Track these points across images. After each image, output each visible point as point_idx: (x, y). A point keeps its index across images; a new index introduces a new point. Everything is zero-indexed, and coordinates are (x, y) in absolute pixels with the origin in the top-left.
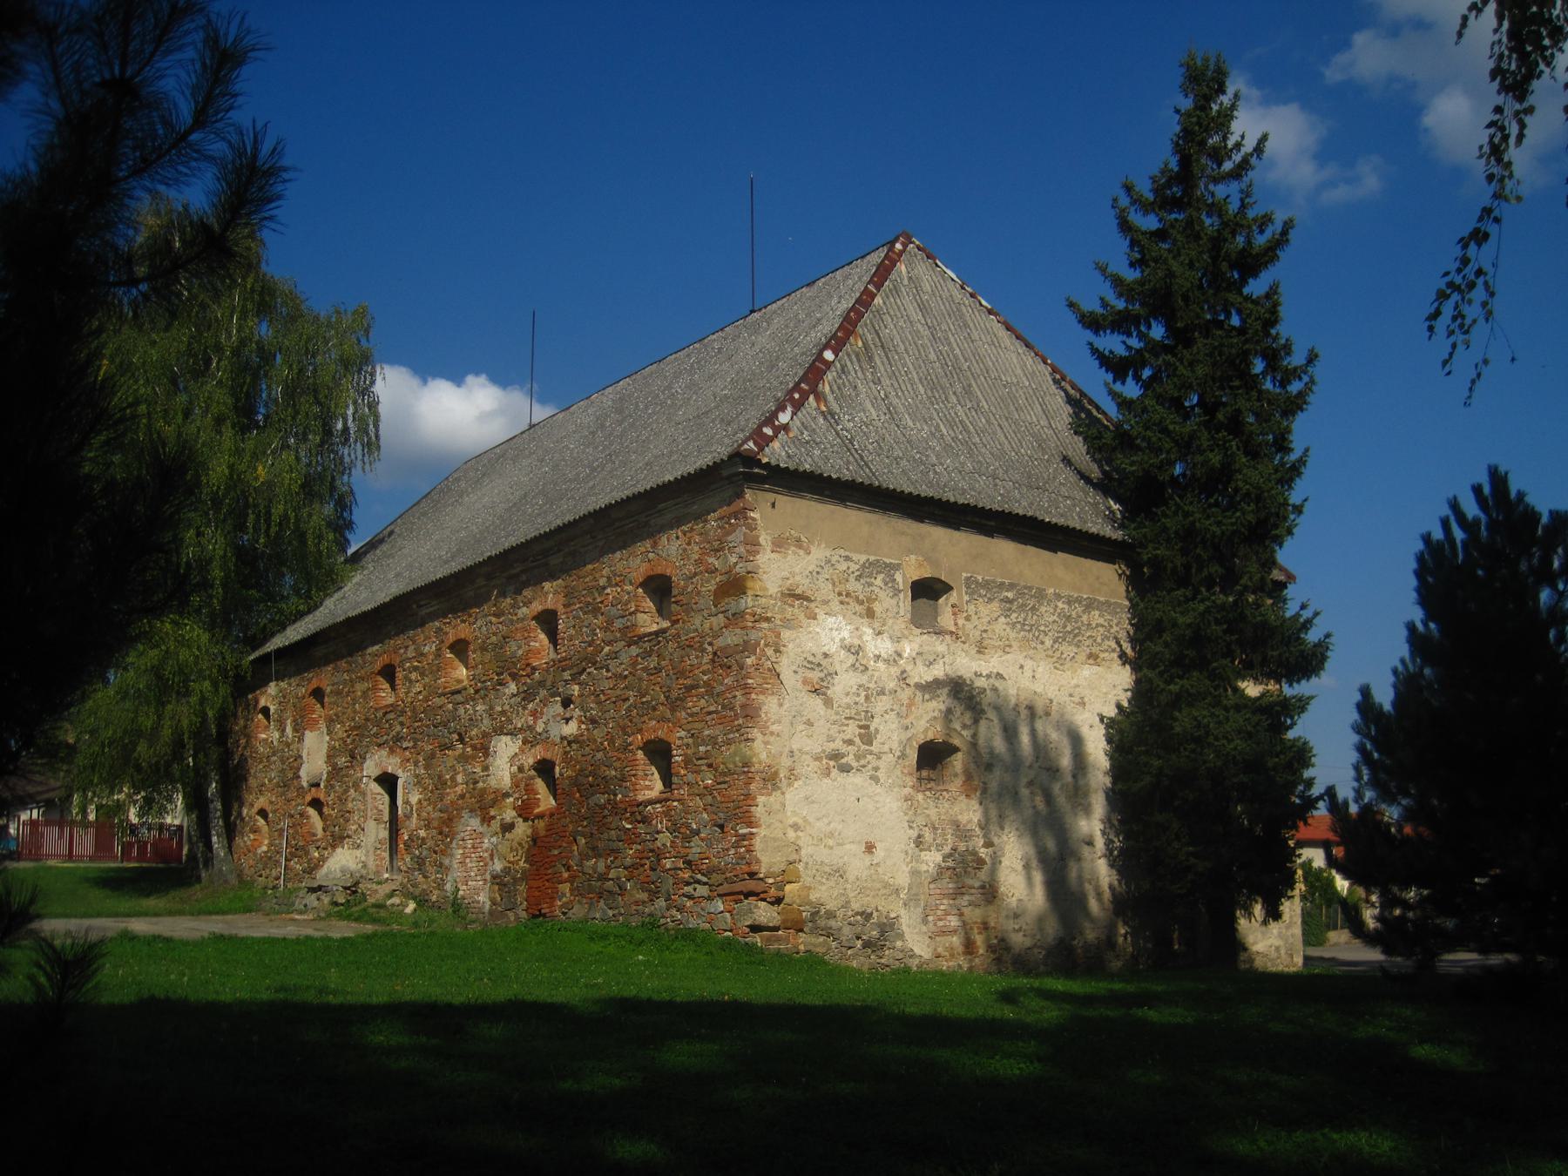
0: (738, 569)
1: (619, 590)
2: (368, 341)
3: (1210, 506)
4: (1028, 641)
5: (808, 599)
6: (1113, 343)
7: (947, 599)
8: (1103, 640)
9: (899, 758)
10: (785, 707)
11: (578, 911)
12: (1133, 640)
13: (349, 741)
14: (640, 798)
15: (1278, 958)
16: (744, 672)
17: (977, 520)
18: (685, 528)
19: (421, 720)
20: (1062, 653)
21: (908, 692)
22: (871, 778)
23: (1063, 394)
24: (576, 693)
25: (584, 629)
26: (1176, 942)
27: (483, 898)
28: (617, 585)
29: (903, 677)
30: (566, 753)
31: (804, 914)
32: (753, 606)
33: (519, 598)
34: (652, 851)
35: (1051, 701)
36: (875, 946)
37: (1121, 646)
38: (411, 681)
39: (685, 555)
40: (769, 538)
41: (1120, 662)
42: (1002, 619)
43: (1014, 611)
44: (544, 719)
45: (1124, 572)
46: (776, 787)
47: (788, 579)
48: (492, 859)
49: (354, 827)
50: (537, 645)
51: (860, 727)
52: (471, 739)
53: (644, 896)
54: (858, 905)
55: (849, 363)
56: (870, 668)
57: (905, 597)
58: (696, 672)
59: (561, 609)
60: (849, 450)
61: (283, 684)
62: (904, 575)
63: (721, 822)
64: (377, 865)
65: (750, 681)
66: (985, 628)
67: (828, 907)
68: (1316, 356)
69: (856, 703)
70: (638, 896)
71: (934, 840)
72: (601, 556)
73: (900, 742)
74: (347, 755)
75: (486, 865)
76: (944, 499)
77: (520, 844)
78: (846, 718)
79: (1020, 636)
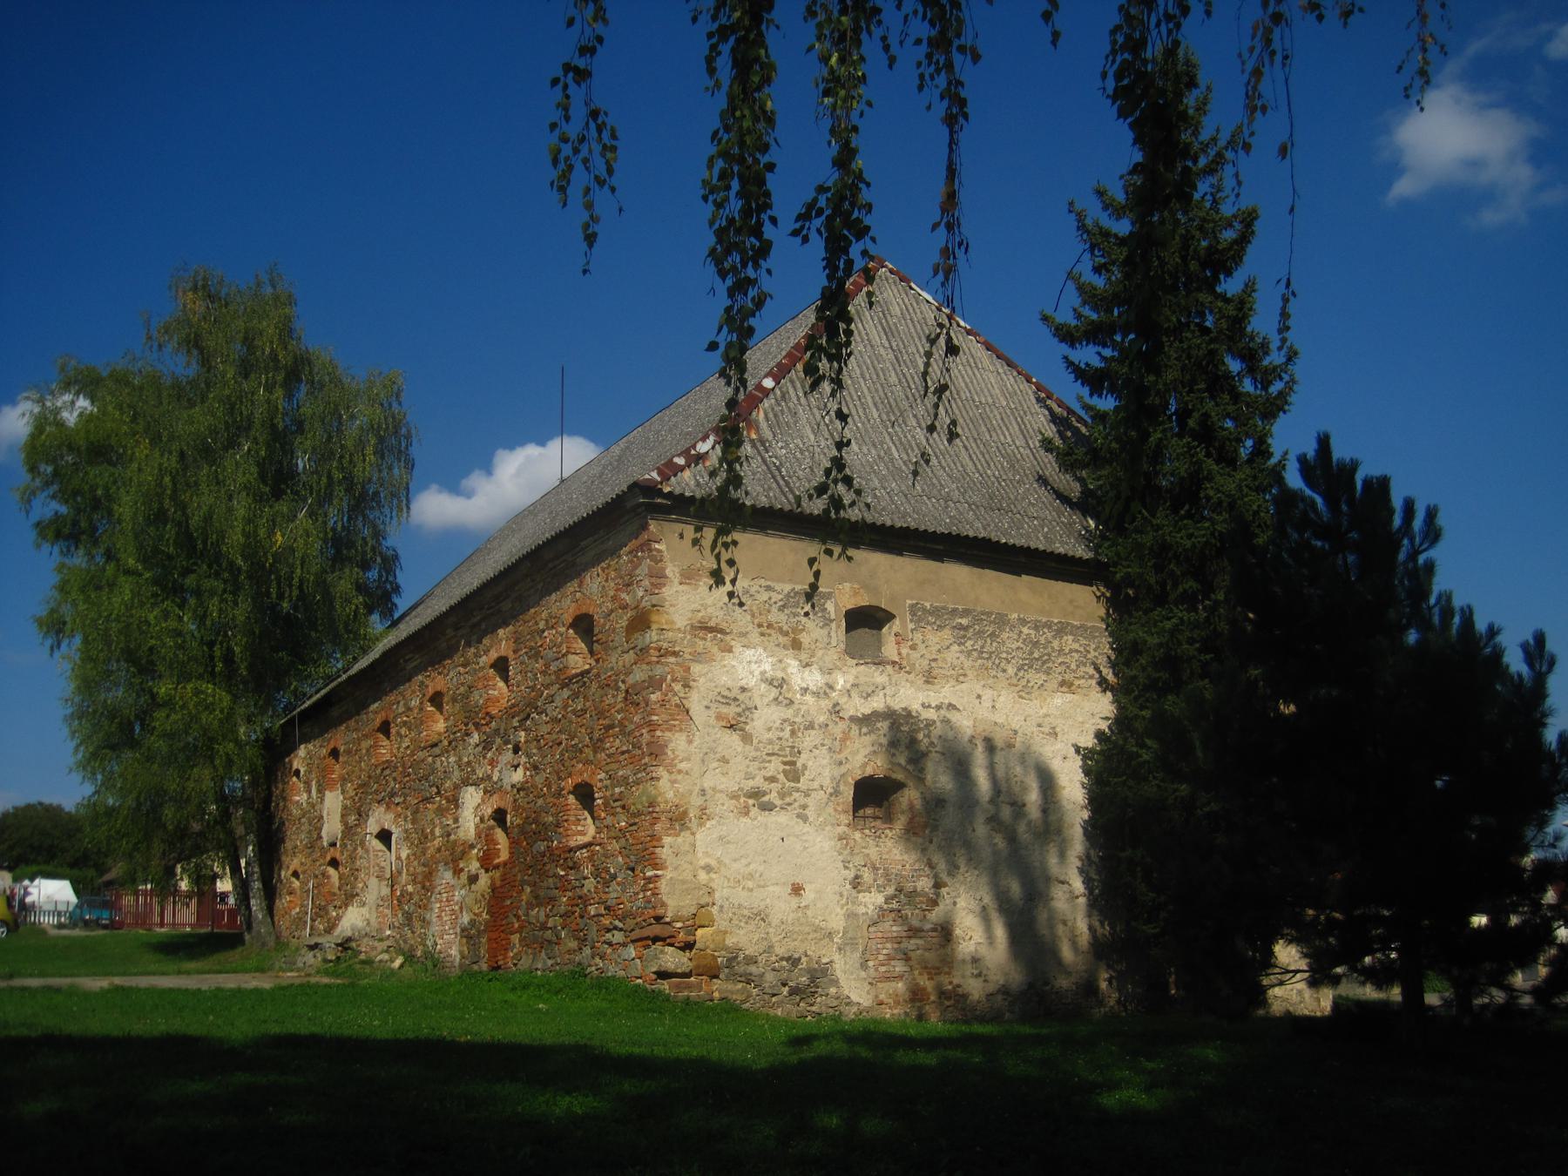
0: (643, 604)
1: (554, 632)
2: (400, 404)
3: (1182, 518)
4: (986, 669)
5: (722, 631)
6: (1088, 355)
7: (890, 628)
8: (1078, 666)
9: (831, 795)
10: (695, 744)
11: (525, 963)
12: (1113, 665)
13: (357, 798)
14: (572, 844)
15: (1301, 1002)
16: (649, 709)
17: (922, 544)
18: (603, 565)
19: (409, 775)
20: (1028, 681)
21: (842, 726)
22: (798, 816)
23: (1047, 413)
24: (522, 740)
25: (529, 674)
26: (1172, 986)
27: (454, 952)
29: (836, 710)
30: (515, 801)
31: (719, 960)
32: (658, 641)
33: (481, 647)
34: (580, 897)
35: (1016, 732)
36: (804, 992)
37: (1100, 672)
38: (401, 736)
40: (677, 570)
41: (1099, 689)
42: (955, 648)
43: (970, 639)
44: (498, 769)
45: (1103, 594)
46: (684, 827)
47: (699, 611)
48: (461, 912)
49: (360, 885)
50: (496, 693)
51: (785, 763)
52: (446, 792)
53: (573, 944)
54: (783, 950)
55: (791, 391)
56: (797, 702)
57: (838, 626)
58: (613, 711)
59: (511, 656)
60: (774, 477)
61: (310, 746)
62: (836, 605)
63: (632, 865)
65: (655, 718)
66: (934, 657)
67: (747, 953)
68: (1296, 353)
69: (780, 739)
71: (875, 880)
72: (540, 599)
73: (832, 779)
74: (356, 812)
75: (456, 918)
76: (879, 523)
77: (483, 896)
78: (768, 754)
79: (977, 664)
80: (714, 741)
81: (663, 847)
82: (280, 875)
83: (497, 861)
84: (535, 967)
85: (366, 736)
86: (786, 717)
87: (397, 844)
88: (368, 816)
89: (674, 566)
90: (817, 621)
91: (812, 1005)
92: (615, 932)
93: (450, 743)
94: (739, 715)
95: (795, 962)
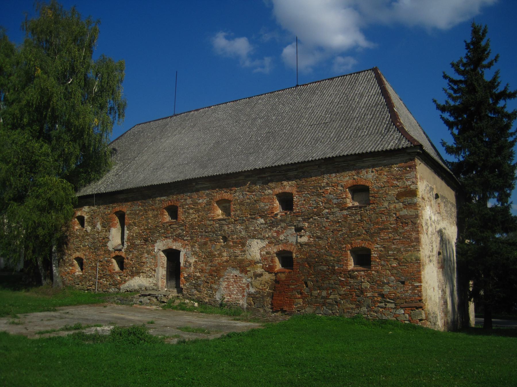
28: (333, 186)
39: (377, 179)
59: (295, 193)
64: (162, 285)
70: (349, 306)
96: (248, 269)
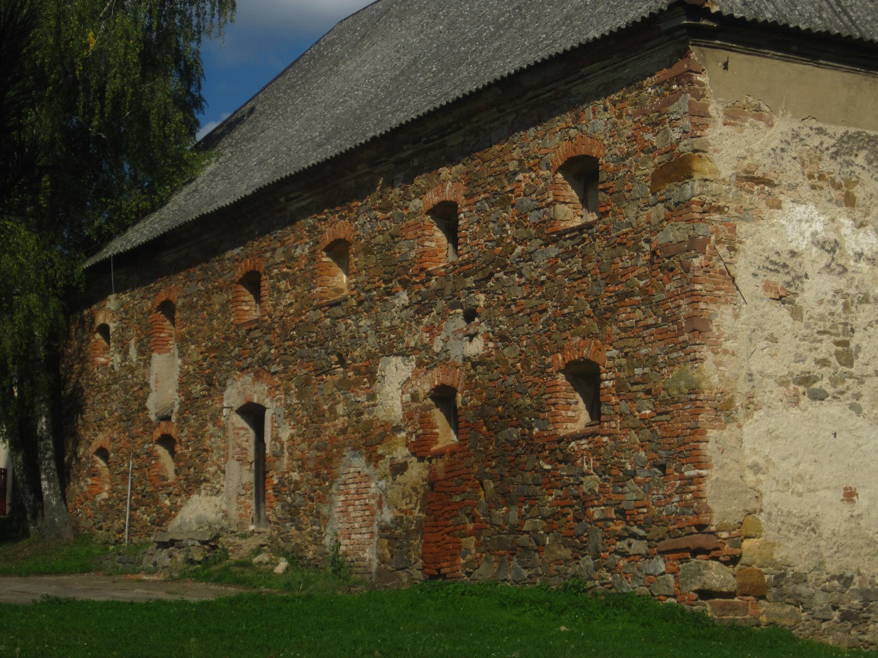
0: (681, 147)
5: (770, 183)
10: (742, 318)
11: (485, 571)
13: (205, 364)
14: (562, 432)
16: (690, 276)
18: (615, 97)
22: (852, 407)
24: (482, 304)
25: (491, 225)
30: (470, 377)
31: (766, 577)
34: (576, 497)
38: (279, 291)
39: (614, 130)
46: (730, 419)
47: (745, 158)
48: (380, 507)
49: (212, 469)
50: (433, 244)
51: (837, 343)
52: (354, 361)
56: (850, 270)
59: (461, 201)
61: (125, 297)
63: (661, 461)
64: (241, 515)
65: (698, 287)
67: (796, 569)
72: (511, 135)
75: (373, 514)
77: (414, 489)
78: (819, 333)
80: (762, 316)
81: (707, 442)
82: (75, 453)
83: (434, 448)
84: (501, 577)
85: (220, 289)
86: (838, 288)
87: (273, 421)
88: (225, 385)
89: (718, 102)
90: (872, 172)
91: (864, 633)
92: (632, 540)
93: (360, 303)
94: (789, 284)
95: (847, 581)
96: (380, 451)
